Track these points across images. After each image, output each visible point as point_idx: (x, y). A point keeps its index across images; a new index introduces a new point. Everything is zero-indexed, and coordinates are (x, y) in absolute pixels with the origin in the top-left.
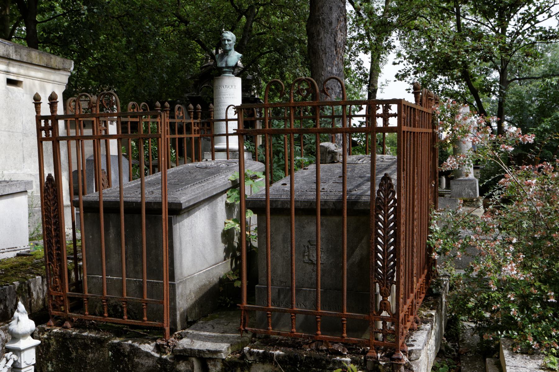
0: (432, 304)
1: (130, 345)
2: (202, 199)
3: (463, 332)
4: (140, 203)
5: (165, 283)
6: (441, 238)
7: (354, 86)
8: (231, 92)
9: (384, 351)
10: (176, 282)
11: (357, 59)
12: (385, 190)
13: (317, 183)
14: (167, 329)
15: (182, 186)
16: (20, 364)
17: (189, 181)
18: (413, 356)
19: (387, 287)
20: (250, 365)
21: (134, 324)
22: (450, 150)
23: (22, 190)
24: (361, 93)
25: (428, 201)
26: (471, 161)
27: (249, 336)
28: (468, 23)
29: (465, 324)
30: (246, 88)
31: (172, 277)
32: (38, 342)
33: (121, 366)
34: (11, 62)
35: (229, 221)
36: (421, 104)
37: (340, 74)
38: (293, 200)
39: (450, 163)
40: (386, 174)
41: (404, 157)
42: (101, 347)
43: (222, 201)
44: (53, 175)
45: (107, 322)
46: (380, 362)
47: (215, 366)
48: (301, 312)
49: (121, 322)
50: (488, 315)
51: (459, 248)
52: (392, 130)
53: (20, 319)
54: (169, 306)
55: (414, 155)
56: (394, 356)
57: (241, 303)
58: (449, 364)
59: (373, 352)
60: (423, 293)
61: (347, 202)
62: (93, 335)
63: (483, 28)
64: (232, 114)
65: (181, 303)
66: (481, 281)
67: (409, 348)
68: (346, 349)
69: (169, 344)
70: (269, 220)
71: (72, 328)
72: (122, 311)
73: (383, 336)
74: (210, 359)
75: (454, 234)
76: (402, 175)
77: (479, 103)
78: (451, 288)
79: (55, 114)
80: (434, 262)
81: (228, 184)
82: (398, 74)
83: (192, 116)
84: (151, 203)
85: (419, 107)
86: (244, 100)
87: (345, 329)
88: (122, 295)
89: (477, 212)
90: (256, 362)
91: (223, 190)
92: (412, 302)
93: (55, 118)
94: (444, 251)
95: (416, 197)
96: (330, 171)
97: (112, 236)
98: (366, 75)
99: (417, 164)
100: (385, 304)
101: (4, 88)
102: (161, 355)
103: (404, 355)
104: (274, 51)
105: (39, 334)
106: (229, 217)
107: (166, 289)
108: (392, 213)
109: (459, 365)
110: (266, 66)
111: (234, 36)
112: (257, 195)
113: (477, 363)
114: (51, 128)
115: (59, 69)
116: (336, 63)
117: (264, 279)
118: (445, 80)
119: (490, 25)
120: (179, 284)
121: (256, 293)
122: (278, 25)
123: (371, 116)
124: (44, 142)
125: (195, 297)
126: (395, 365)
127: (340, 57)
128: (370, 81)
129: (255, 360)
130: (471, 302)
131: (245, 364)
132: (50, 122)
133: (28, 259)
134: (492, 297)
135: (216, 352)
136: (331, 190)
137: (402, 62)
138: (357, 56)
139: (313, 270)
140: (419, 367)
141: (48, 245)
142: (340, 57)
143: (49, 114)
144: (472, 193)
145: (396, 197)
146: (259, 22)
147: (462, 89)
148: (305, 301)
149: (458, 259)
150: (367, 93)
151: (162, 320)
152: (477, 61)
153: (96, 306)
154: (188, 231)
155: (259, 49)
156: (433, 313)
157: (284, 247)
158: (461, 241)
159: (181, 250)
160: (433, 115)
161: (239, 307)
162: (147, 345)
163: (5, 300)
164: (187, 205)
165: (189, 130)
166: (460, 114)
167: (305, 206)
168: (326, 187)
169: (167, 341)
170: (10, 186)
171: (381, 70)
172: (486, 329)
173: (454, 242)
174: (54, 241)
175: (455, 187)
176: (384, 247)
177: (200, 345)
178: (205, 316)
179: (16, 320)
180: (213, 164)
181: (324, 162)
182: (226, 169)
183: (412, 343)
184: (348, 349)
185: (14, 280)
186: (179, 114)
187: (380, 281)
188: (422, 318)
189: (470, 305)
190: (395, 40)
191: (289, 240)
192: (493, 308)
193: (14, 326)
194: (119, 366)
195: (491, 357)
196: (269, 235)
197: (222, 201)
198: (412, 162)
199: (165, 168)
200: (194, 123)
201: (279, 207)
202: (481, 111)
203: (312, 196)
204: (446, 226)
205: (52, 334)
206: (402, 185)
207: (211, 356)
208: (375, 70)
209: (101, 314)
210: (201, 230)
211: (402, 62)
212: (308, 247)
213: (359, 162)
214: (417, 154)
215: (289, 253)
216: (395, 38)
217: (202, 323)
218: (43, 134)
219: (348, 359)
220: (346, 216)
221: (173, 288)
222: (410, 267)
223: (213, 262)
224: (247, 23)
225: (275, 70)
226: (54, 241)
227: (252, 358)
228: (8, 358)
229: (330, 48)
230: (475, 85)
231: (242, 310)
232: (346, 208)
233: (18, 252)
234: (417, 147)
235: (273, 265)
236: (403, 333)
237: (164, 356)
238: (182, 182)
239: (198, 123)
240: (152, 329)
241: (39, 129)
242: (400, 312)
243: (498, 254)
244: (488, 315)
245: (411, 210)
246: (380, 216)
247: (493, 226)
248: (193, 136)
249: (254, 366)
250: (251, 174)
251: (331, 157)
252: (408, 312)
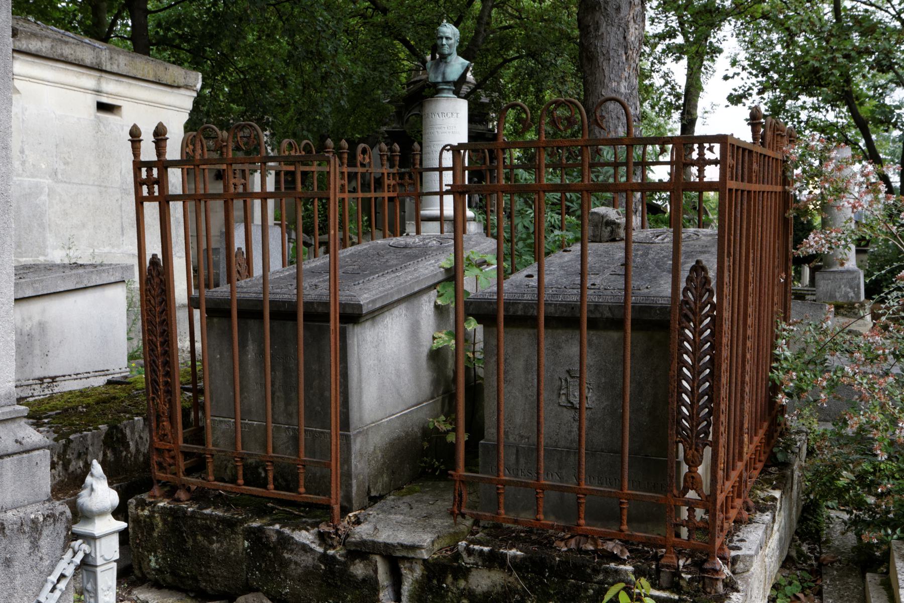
0: (776, 479)
1: (278, 532)
2: (396, 298)
3: (828, 527)
4: (261, 302)
5: (333, 434)
6: (794, 370)
7: (658, 115)
8: (451, 123)
9: (691, 555)
10: (352, 432)
11: (664, 68)
12: (696, 288)
13: (582, 274)
14: (337, 509)
15: (365, 276)
16: (95, 559)
17: (377, 268)
18: (740, 566)
19: (697, 450)
20: (469, 570)
21: (284, 498)
22: (817, 221)
23: (118, 279)
24: (669, 127)
25: (773, 307)
26: (849, 240)
27: (469, 522)
28: (853, 7)
29: (833, 514)
30: (476, 117)
31: (345, 424)
32: (122, 525)
33: (264, 565)
34: (104, 75)
35: (440, 335)
36: (763, 144)
37: (631, 93)
38: (543, 303)
39: (813, 242)
40: (698, 262)
41: (729, 234)
42: (232, 533)
43: (430, 302)
44: (160, 256)
45: (242, 494)
46: (683, 575)
47: (412, 570)
48: (552, 488)
49: (264, 495)
50: (871, 500)
51: (824, 388)
52: (711, 186)
53: (94, 487)
54: (339, 472)
55: (748, 230)
56: (707, 566)
57: (454, 469)
58: (802, 581)
59: (672, 558)
60: (760, 461)
61: (633, 307)
62: (219, 513)
63: (880, 15)
64: (448, 159)
65: (359, 466)
66: (862, 442)
67: (733, 553)
68: (626, 551)
69: (340, 532)
70: (502, 334)
71: (188, 500)
72: (266, 477)
73: (689, 531)
74: (404, 558)
75: (817, 363)
76: (726, 264)
77: (869, 142)
78: (810, 453)
79: (162, 158)
80: (783, 409)
81: (440, 275)
82: (731, 94)
83: (346, 161)
84: (312, 303)
85: (759, 149)
86: (472, 136)
87: (625, 518)
88: (266, 451)
89: (860, 326)
90: (478, 566)
91: (431, 283)
92: (740, 476)
93: (164, 165)
94: (800, 390)
95: (750, 299)
96: (604, 255)
97: (251, 355)
98: (678, 96)
99: (753, 245)
100: (693, 477)
101: (93, 118)
102: (326, 550)
103: (724, 563)
104: (528, 55)
105: (136, 508)
106: (439, 329)
107: (335, 442)
108: (708, 326)
109: (819, 582)
110: (512, 81)
111: (456, 30)
112: (484, 293)
113: (850, 580)
114: (157, 182)
115: (179, 87)
116: (627, 75)
117: (494, 431)
118: (813, 103)
119: (891, 10)
120: (356, 435)
121: (480, 453)
122: (533, 12)
123: (680, 165)
124: (146, 204)
125: (383, 457)
126: (707, 581)
127: (634, 65)
128: (684, 105)
129: (476, 564)
130: (843, 477)
131: (460, 567)
132: (155, 172)
133: (124, 390)
134: (880, 470)
135: (413, 548)
136: (605, 284)
137: (738, 74)
138: (664, 64)
139: (574, 418)
140: (748, 585)
141: (151, 367)
142: (634, 65)
143: (155, 158)
144: (852, 294)
145: (715, 299)
146: (502, 8)
147: (841, 118)
148: (560, 468)
149: (822, 404)
150: (680, 124)
151: (327, 492)
152: (868, 72)
153: (226, 467)
154: (372, 349)
155: (502, 52)
156: (777, 494)
157: (527, 379)
158: (827, 375)
159: (360, 381)
160: (785, 162)
161: (452, 475)
162: (304, 532)
163: (86, 454)
164: (371, 307)
165: (379, 183)
166: (831, 159)
167: (562, 312)
168: (598, 282)
169: (335, 527)
170: (99, 273)
171: (704, 86)
172: (868, 524)
173: (815, 376)
174: (160, 362)
175: (824, 284)
176: (694, 383)
177: (389, 536)
178: (399, 489)
179: (89, 488)
180: (417, 240)
181: (596, 239)
182: (438, 249)
183: (738, 544)
184: (630, 551)
185: (100, 421)
186: (364, 159)
187: (686, 441)
188: (758, 502)
189: (842, 482)
190: (729, 37)
191: (535, 368)
192: (879, 490)
193: (85, 499)
194: (260, 565)
195: (874, 571)
196: (502, 360)
197: (430, 302)
198: (744, 241)
199: (335, 247)
200: (388, 174)
201: (519, 313)
202: (872, 156)
203: (573, 296)
204: (803, 349)
205: (156, 509)
206: (726, 280)
207: (405, 554)
208: (693, 88)
209: (234, 480)
210: (395, 349)
211: (738, 74)
212: (566, 380)
213: (656, 240)
214: (754, 228)
215: (536, 389)
216: (729, 35)
217: (393, 500)
218: (145, 190)
219: (629, 568)
220: (629, 330)
221: (347, 441)
222: (738, 419)
223: (414, 402)
224: (482, 11)
225: (528, 88)
226: (160, 362)
227: (471, 560)
228: (76, 548)
229: (616, 51)
230: (864, 111)
231: (455, 481)
232: (629, 317)
233: (110, 377)
234: (754, 217)
235: (509, 408)
236: (722, 527)
237: (331, 552)
238: (364, 270)
239: (394, 174)
240: (312, 507)
241: (138, 183)
242: (719, 492)
243: (891, 399)
244: (871, 500)
245: (741, 322)
246: (687, 331)
247: (884, 352)
248: (386, 195)
249: (474, 572)
250: (476, 258)
251: (608, 231)
252: (733, 492)
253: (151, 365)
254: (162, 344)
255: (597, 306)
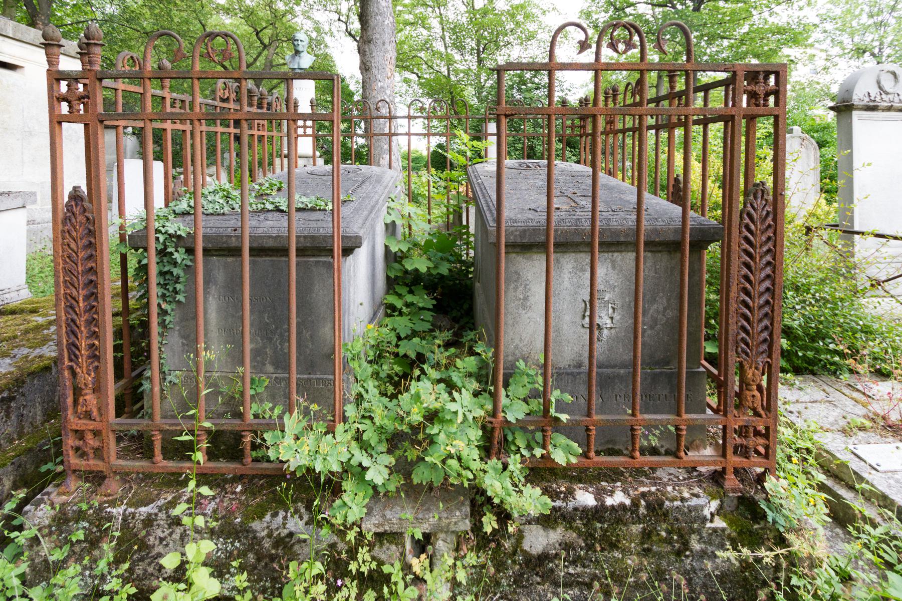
44: (84, 188)
143: (310, 111)
226: (82, 321)
232: (688, 240)
241: (55, 99)
253: (68, 325)
254: (87, 298)
255: (656, 231)
